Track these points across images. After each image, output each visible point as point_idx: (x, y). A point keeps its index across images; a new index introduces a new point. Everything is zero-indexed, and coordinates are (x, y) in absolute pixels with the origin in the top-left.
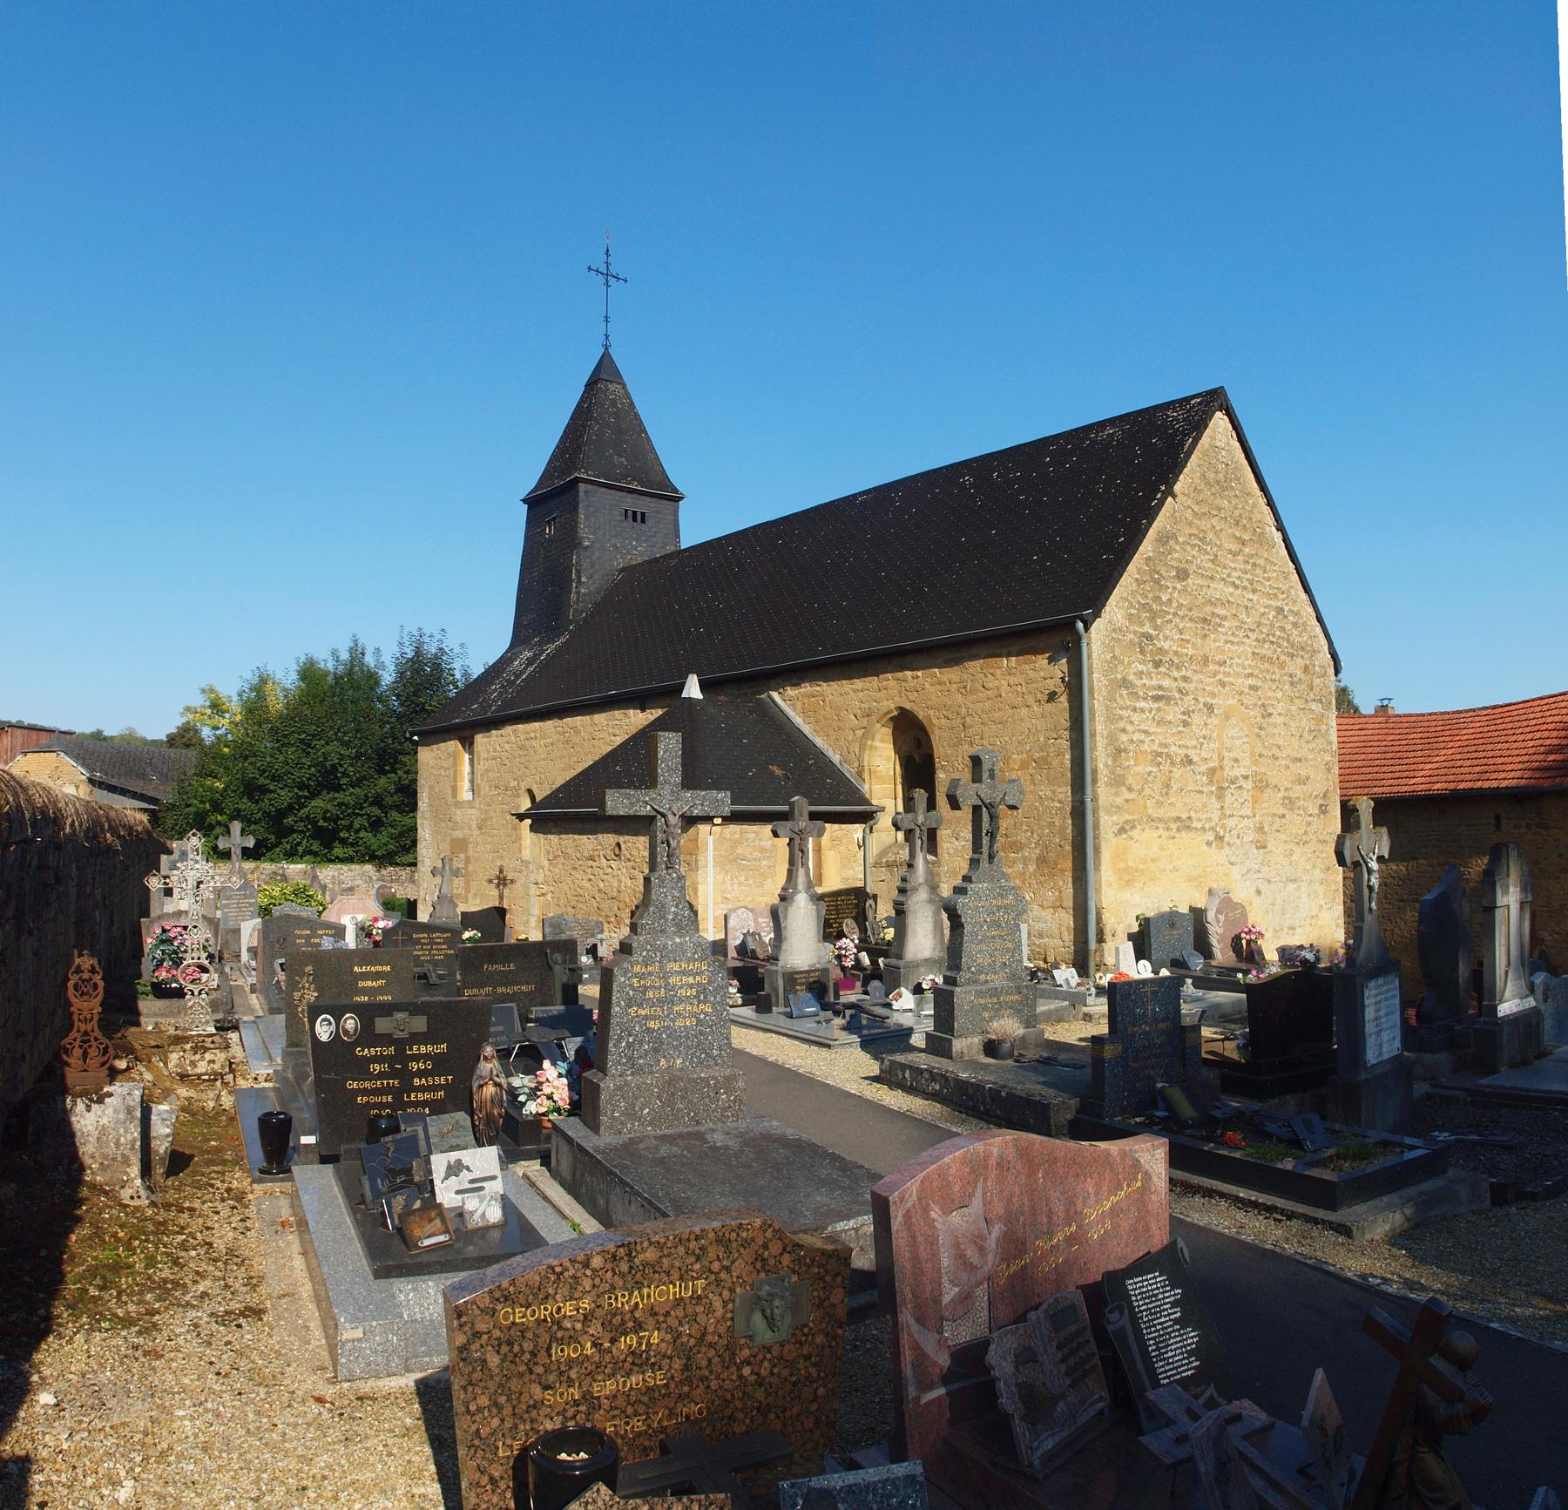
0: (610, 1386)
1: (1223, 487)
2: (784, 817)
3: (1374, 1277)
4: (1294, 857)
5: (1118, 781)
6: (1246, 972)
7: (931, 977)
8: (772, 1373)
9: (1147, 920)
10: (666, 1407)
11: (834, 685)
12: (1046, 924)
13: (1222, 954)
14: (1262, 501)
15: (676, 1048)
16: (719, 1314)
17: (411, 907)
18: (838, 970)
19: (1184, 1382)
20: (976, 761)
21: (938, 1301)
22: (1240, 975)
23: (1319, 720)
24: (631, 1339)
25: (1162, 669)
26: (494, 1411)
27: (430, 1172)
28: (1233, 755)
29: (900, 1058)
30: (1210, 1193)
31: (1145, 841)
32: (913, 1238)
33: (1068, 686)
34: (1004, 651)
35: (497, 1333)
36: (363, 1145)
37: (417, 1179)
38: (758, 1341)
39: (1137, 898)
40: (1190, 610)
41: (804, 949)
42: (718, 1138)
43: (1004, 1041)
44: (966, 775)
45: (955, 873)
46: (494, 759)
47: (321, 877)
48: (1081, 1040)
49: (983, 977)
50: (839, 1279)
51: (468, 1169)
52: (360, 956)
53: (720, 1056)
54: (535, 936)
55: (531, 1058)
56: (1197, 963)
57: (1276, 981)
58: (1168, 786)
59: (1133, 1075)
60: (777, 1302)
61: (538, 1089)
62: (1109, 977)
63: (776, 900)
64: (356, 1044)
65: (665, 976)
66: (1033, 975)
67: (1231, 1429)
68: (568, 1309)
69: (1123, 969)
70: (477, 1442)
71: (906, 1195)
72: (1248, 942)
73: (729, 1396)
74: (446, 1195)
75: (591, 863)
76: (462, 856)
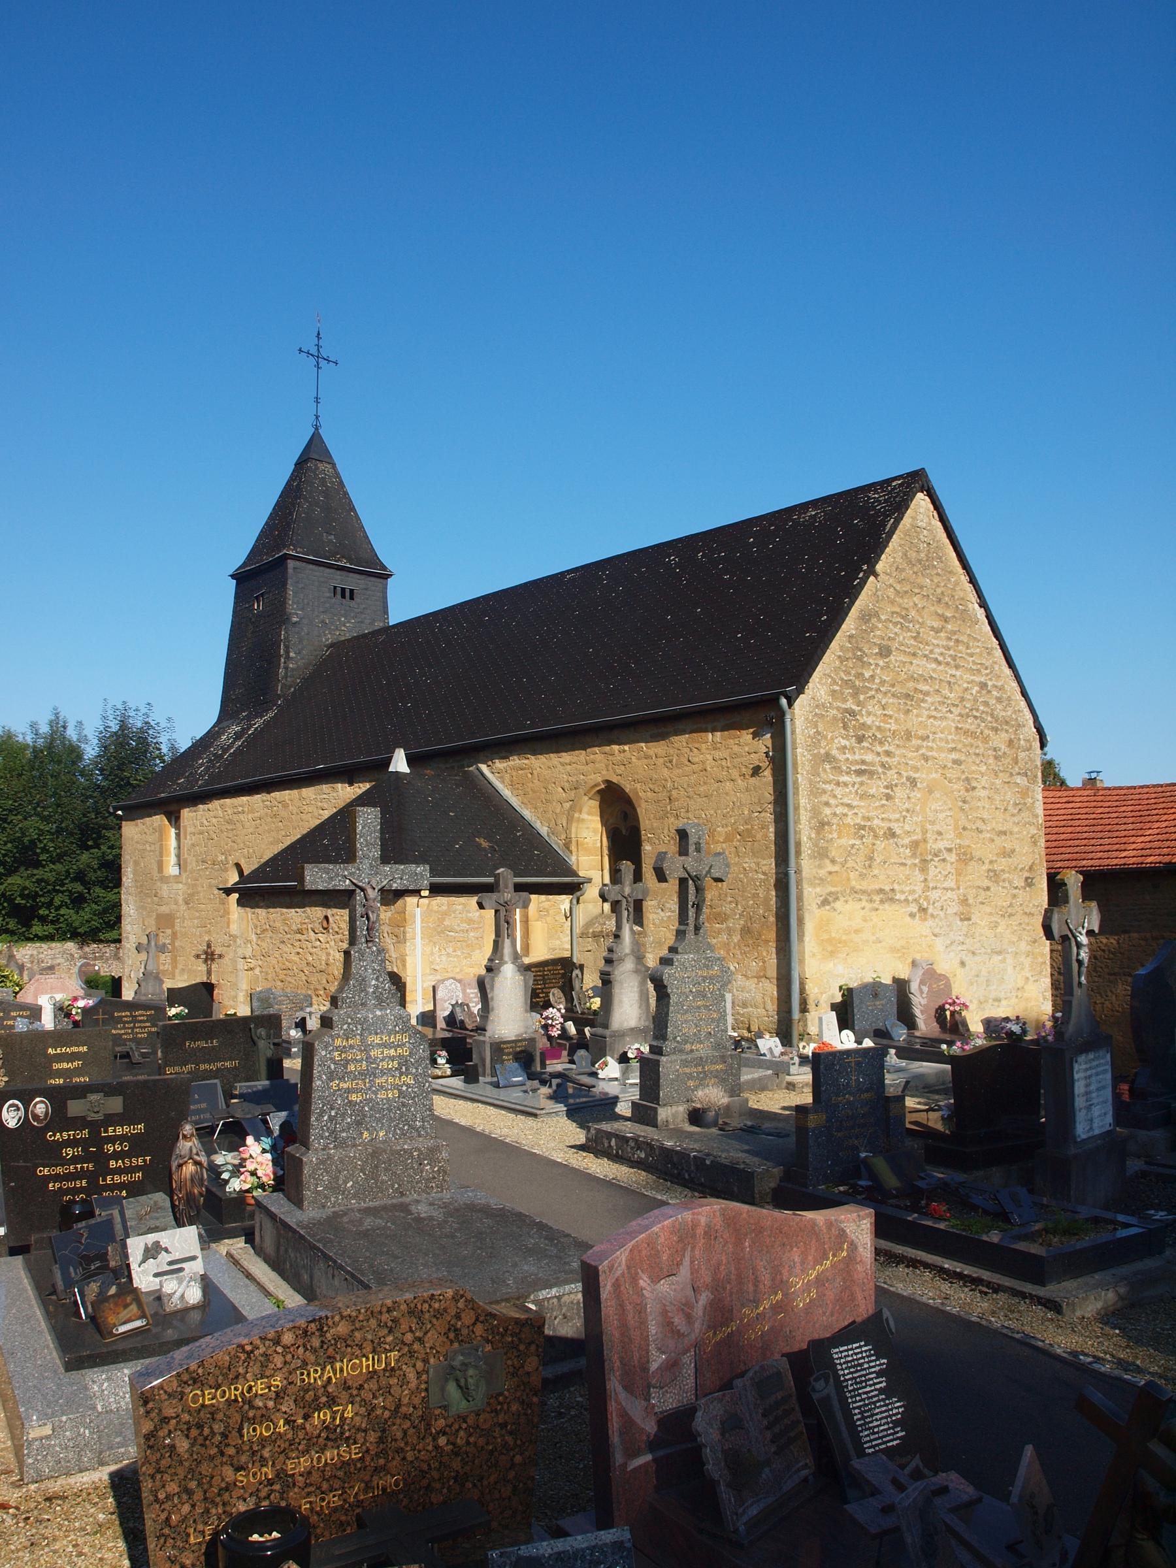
0: (304, 1463)
1: (925, 565)
2: (489, 888)
3: (1086, 1355)
4: (1000, 929)
5: (821, 854)
6: (950, 1044)
7: (637, 1046)
8: (468, 1443)
9: (850, 990)
10: (362, 1481)
11: (542, 758)
12: (750, 994)
13: (926, 1025)
14: (964, 579)
15: (379, 1120)
16: (413, 1385)
17: (116, 985)
18: (545, 1040)
19: (889, 1452)
20: (683, 834)
21: (645, 1368)
22: (944, 1047)
23: (1025, 793)
24: (325, 1415)
25: (865, 744)
26: (185, 1497)
27: (127, 1256)
28: (937, 828)
29: (606, 1127)
30: (914, 1263)
31: (849, 913)
32: (621, 1306)
33: (772, 760)
34: (710, 726)
35: (186, 1417)
36: (55, 1233)
37: (112, 1264)
38: (453, 1411)
39: (840, 969)
40: (893, 686)
41: (511, 1019)
42: (423, 1210)
43: (708, 1109)
44: (672, 848)
45: (660, 944)
46: (201, 833)
47: (18, 956)
48: (784, 1108)
49: (688, 1047)
50: (533, 1347)
51: (166, 1250)
52: (56, 1037)
53: (423, 1127)
54: (244, 1011)
55: (235, 1135)
56: (901, 1034)
57: (981, 1053)
58: (871, 859)
59: (836, 1144)
60: (471, 1372)
61: (241, 1165)
62: (813, 1046)
63: (483, 972)
64: (47, 1128)
65: (366, 1048)
66: (737, 1043)
67: (938, 1501)
68: (259, 1387)
69: (826, 1039)
70: (166, 1531)
71: (615, 1263)
72: (953, 1013)
73: (425, 1467)
74: (144, 1278)
75: (299, 936)
76: (169, 931)
